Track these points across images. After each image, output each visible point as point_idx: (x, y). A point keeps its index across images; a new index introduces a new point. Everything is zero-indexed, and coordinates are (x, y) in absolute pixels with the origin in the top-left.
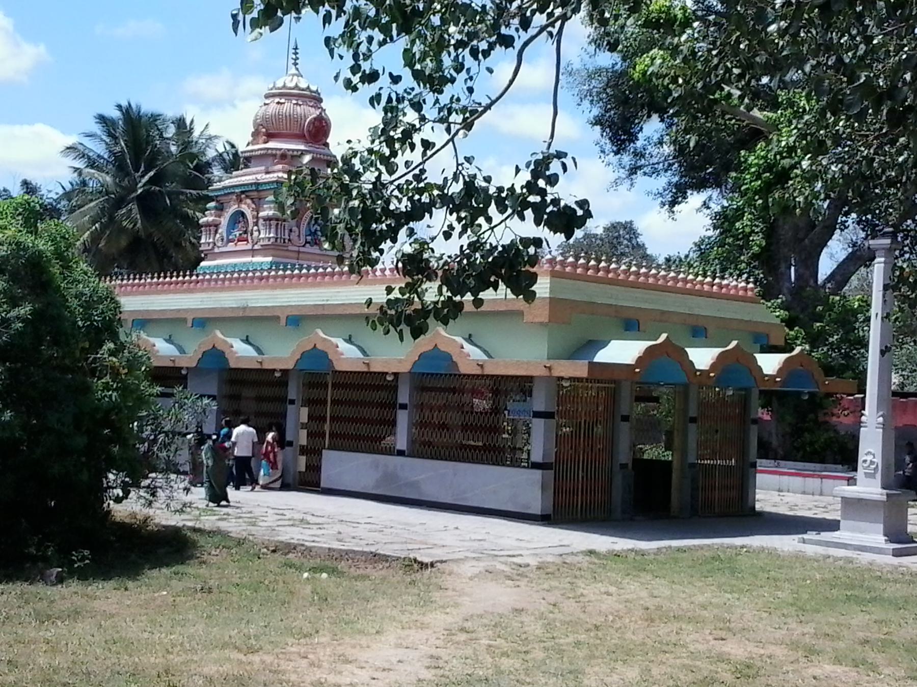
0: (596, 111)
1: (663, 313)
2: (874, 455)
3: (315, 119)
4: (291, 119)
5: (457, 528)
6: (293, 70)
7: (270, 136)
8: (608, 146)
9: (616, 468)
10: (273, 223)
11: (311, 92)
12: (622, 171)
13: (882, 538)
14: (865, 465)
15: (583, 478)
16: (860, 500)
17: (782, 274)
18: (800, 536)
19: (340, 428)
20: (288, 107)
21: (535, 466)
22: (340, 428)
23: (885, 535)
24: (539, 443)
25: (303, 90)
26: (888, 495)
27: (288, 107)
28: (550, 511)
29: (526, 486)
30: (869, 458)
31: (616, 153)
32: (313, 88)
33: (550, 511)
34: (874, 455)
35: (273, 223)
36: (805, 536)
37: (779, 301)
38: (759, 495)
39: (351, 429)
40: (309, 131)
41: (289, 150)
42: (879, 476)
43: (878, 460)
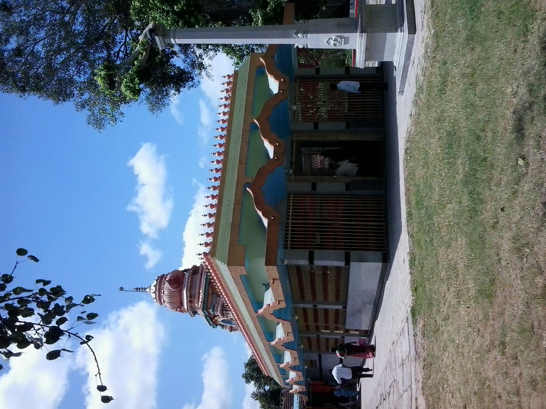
0: (172, 92)
1: (240, 162)
2: (329, 39)
3: (170, 285)
4: (171, 296)
5: (393, 343)
6: (148, 290)
7: (182, 304)
8: (191, 83)
9: (349, 192)
10: (224, 312)
11: (157, 284)
12: (202, 73)
13: (399, 34)
14: (338, 44)
15: (356, 221)
16: (367, 49)
17: (238, 7)
18: (397, 94)
19: (331, 296)
20: (165, 298)
21: (348, 263)
22: (331, 296)
23: (396, 31)
24: (334, 262)
25: (156, 289)
26: (362, 32)
27: (165, 298)
28: (379, 254)
29: (363, 273)
30: (332, 42)
31: (193, 79)
32: (156, 278)
33: (379, 254)
34: (329, 39)
35: (224, 312)
36: (398, 90)
37: (252, 14)
38: (365, 265)
39: (331, 286)
40: (177, 288)
41: (187, 299)
42: (346, 35)
43: (333, 36)
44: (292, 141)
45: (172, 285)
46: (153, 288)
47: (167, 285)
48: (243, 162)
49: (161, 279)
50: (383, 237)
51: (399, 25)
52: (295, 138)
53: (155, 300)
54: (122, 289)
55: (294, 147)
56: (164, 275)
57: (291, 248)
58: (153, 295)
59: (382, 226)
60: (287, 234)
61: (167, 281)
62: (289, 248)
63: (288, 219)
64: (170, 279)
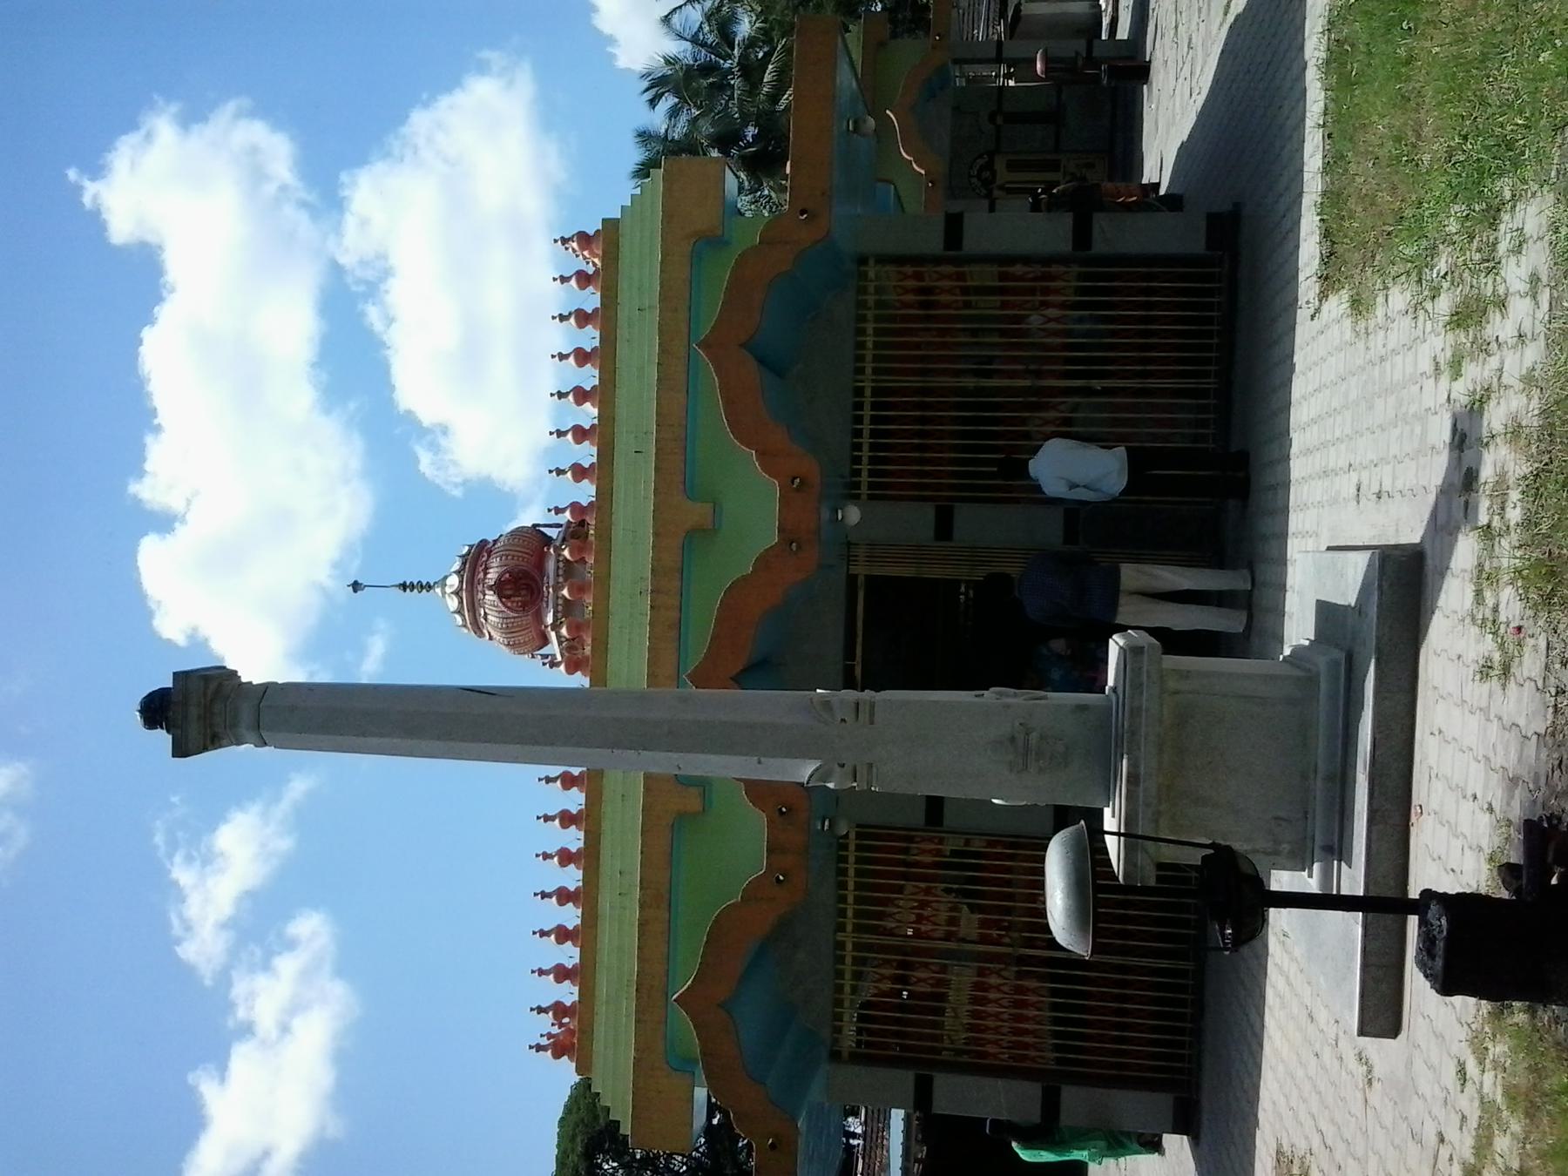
3: (500, 598)
6: (438, 590)
11: (460, 589)
44: (852, 580)
45: (508, 597)
46: (454, 581)
47: (491, 597)
48: (657, 898)
49: (476, 558)
50: (1181, 1031)
51: (1319, 840)
52: (861, 570)
53: (458, 618)
54: (356, 586)
55: (860, 624)
56: (484, 543)
57: (871, 497)
58: (453, 603)
59: (1183, 974)
60: (858, 433)
61: (490, 588)
62: (864, 497)
63: (841, 928)
64: (501, 575)
